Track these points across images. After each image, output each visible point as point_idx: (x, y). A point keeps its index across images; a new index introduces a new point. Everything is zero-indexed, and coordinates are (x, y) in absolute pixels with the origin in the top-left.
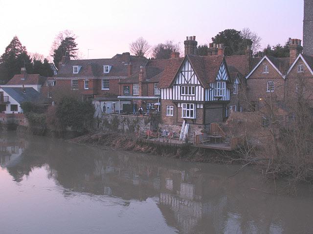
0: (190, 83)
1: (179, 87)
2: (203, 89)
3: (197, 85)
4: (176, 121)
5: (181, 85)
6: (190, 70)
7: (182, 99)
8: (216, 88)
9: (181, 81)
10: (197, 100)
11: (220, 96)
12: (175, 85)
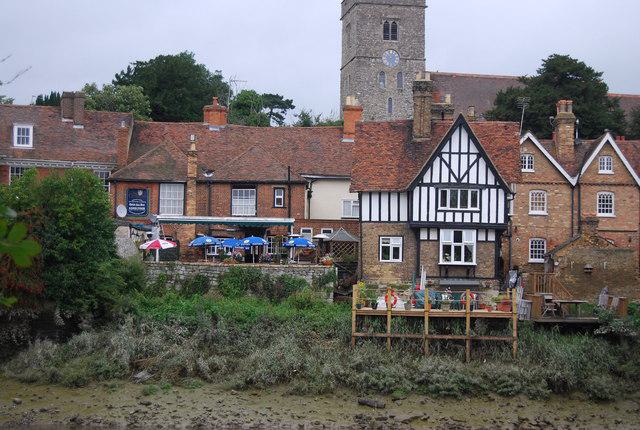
1: (432, 190)
3: (482, 187)
6: (464, 149)
7: (440, 218)
9: (438, 173)
10: (485, 220)
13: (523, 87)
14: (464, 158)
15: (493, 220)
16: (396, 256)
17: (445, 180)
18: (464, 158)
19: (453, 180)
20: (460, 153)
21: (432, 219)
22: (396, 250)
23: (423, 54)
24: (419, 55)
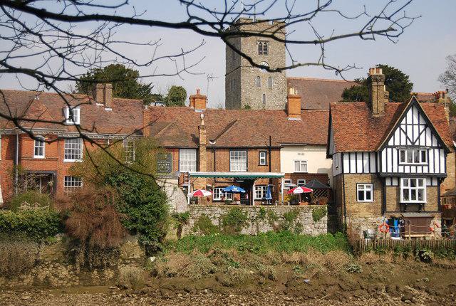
7: (401, 170)
9: (398, 139)
10: (431, 171)
14: (416, 128)
16: (369, 197)
18: (416, 128)
19: (409, 143)
21: (395, 171)
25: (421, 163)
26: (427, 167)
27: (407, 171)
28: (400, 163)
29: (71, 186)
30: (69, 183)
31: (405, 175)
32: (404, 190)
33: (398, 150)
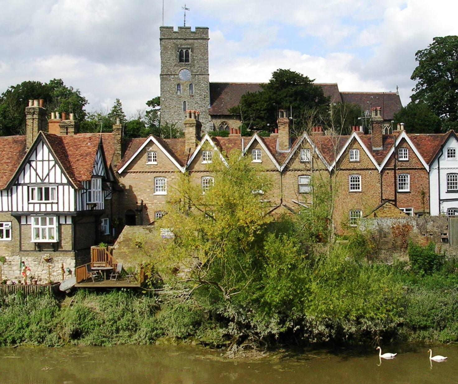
0: (46, 181)
1: (25, 188)
2: (72, 191)
3: (62, 184)
4: (18, 249)
5: (28, 185)
6: (46, 158)
7: (31, 209)
8: (90, 188)
9: (29, 177)
10: (61, 209)
11: (95, 202)
12: (20, 184)
13: (262, 90)
14: (46, 163)
15: (66, 210)
16: (8, 236)
17: (33, 181)
18: (46, 163)
19: (39, 181)
20: (43, 161)
21: (25, 210)
22: (8, 231)
23: (208, 70)
24: (205, 73)
25: (44, 201)
26: (56, 205)
27: (37, 209)
28: (31, 201)
29: (452, 182)
30: (454, 187)
31: (34, 213)
32: (2, 224)
33: (28, 187)
